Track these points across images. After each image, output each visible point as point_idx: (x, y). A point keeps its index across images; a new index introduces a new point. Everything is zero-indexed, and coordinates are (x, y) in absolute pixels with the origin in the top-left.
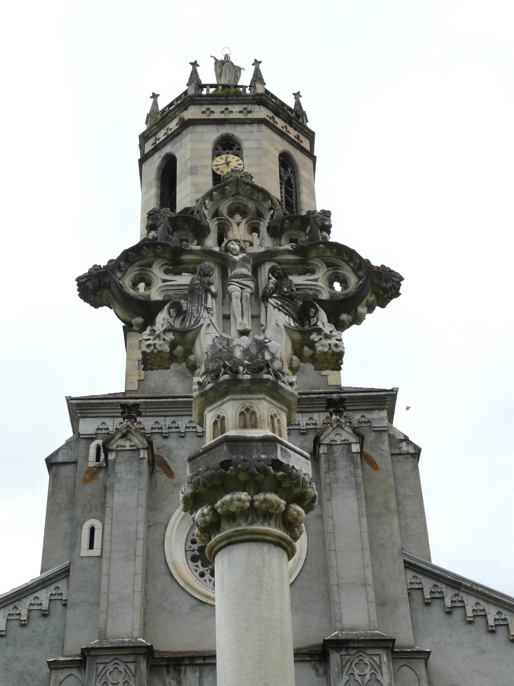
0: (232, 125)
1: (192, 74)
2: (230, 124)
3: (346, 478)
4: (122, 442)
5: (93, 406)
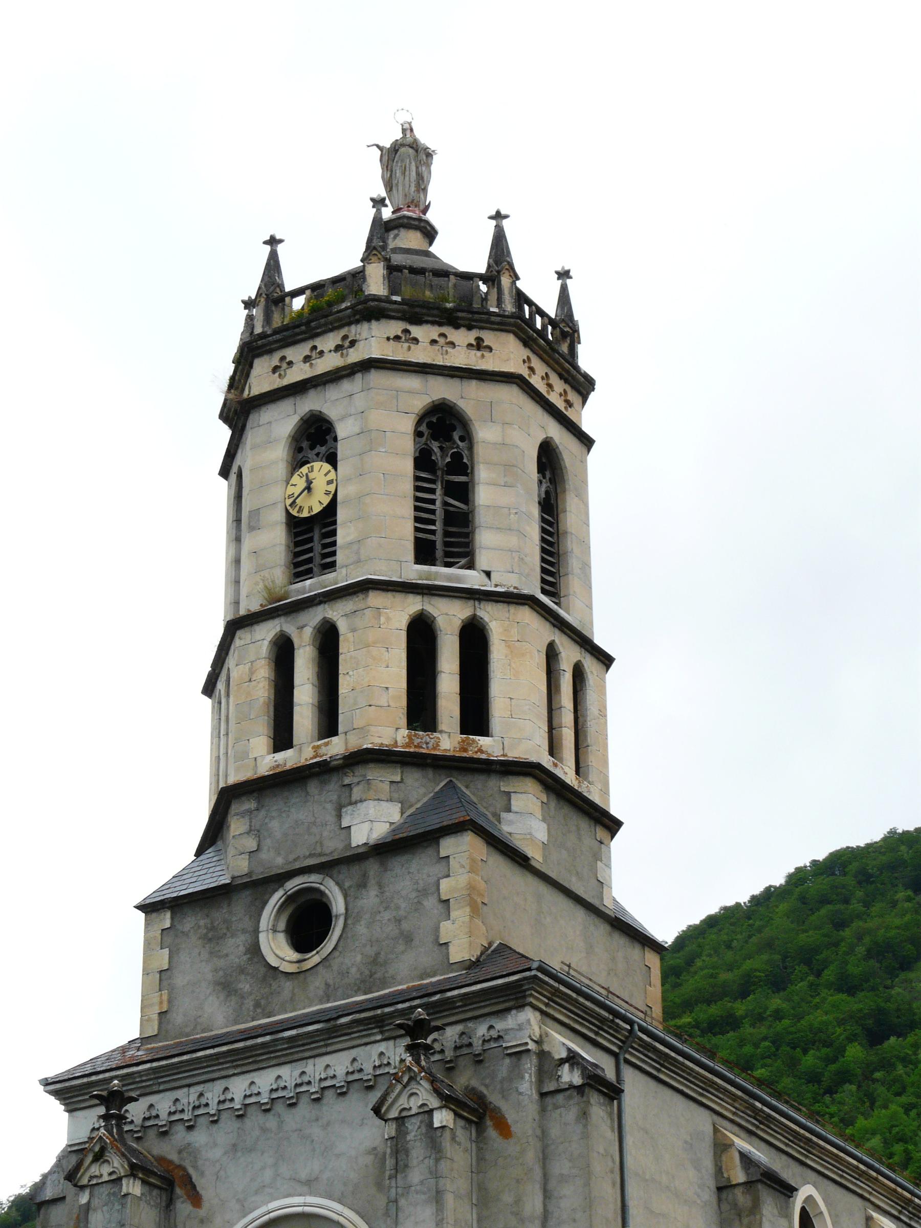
0: (319, 388)
1: (268, 264)
2: (315, 386)
3: (422, 1183)
4: (95, 1170)
5: (80, 1090)
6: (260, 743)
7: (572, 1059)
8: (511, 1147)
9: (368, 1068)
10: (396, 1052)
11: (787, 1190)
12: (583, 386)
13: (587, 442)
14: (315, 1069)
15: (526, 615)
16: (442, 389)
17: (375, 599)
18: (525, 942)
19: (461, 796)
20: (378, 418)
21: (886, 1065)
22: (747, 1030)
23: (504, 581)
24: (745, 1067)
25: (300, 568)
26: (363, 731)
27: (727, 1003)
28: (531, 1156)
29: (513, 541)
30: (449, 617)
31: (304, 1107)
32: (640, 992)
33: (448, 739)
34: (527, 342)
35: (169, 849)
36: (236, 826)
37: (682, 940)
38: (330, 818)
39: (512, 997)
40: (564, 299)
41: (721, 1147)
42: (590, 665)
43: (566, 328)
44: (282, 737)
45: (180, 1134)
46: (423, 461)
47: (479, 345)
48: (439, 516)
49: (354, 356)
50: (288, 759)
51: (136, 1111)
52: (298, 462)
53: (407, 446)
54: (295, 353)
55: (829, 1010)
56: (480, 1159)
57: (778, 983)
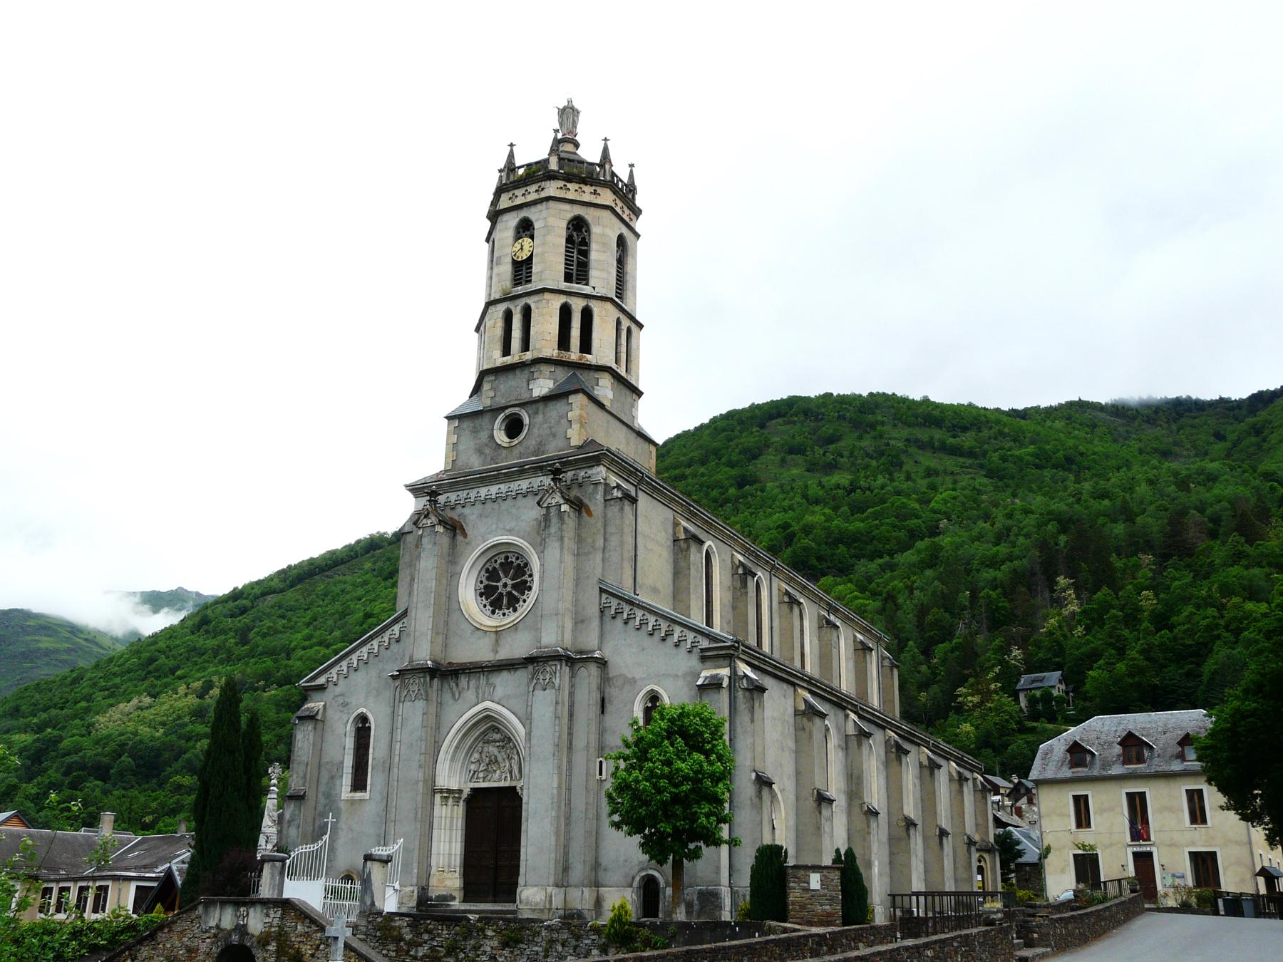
6: (497, 353)
7: (618, 487)
8: (592, 521)
9: (524, 487)
10: (547, 481)
11: (702, 542)
12: (637, 212)
13: (638, 236)
14: (514, 486)
15: (609, 306)
16: (578, 211)
17: (547, 296)
18: (602, 439)
19: (578, 379)
20: (552, 221)
21: (745, 497)
22: (690, 480)
23: (600, 291)
24: (689, 495)
25: (517, 281)
26: (540, 350)
27: (683, 469)
28: (600, 525)
29: (605, 275)
30: (577, 305)
31: (509, 500)
32: (647, 462)
33: (574, 355)
34: (615, 193)
35: (459, 394)
36: (486, 386)
37: (666, 444)
38: (525, 385)
39: (596, 461)
40: (631, 176)
41: (676, 524)
42: (634, 327)
43: (631, 188)
44: (506, 351)
45: (459, 509)
46: (569, 240)
47: (595, 193)
48: (575, 263)
49: (543, 195)
50: (508, 360)
51: (442, 499)
52: (518, 237)
53: (564, 233)
54: (519, 192)
55: (723, 474)
56: (579, 524)
57: (703, 462)
